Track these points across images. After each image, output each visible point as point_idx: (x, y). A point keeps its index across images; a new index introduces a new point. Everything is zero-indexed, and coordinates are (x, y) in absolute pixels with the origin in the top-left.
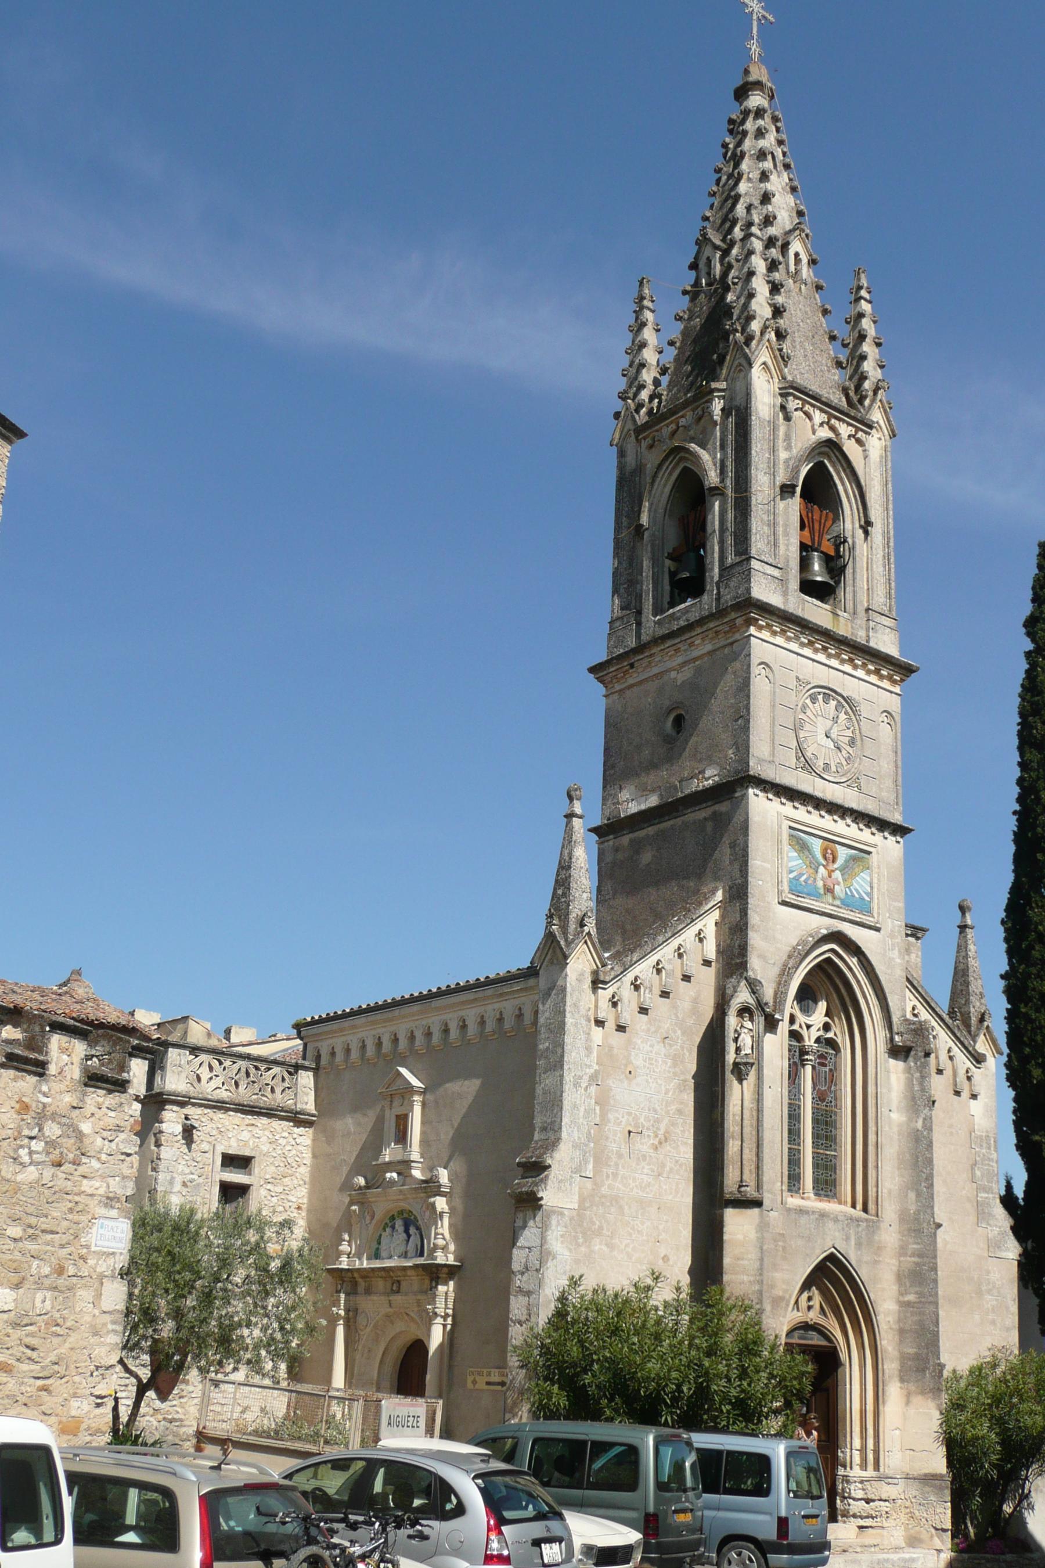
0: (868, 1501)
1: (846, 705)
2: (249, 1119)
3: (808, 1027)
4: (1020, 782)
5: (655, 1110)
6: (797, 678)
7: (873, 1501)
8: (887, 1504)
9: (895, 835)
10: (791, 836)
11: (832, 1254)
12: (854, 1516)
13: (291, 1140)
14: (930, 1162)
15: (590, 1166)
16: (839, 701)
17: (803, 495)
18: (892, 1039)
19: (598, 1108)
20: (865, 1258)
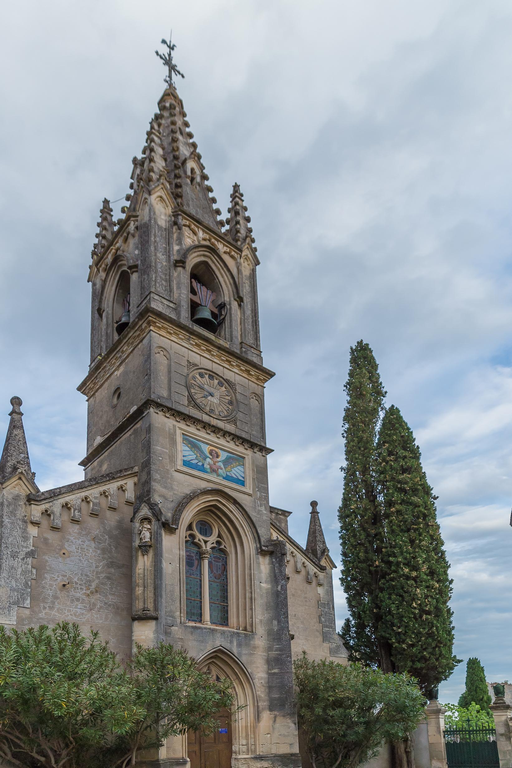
1: (225, 383)
5: (87, 575)
6: (188, 361)
15: (28, 601)
18: (261, 548)
20: (244, 652)
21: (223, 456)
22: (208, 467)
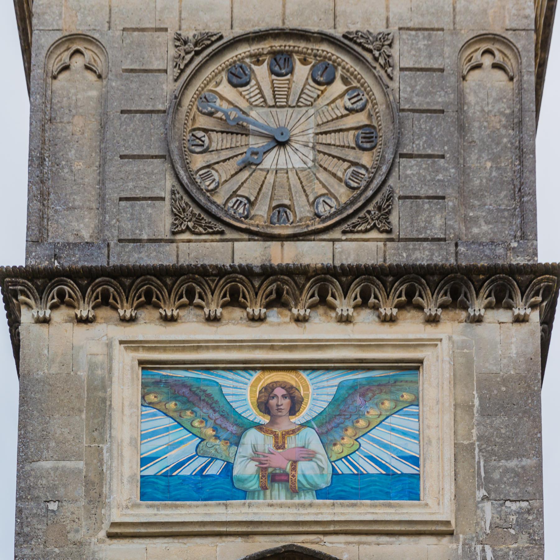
21: (318, 392)
22: (252, 468)
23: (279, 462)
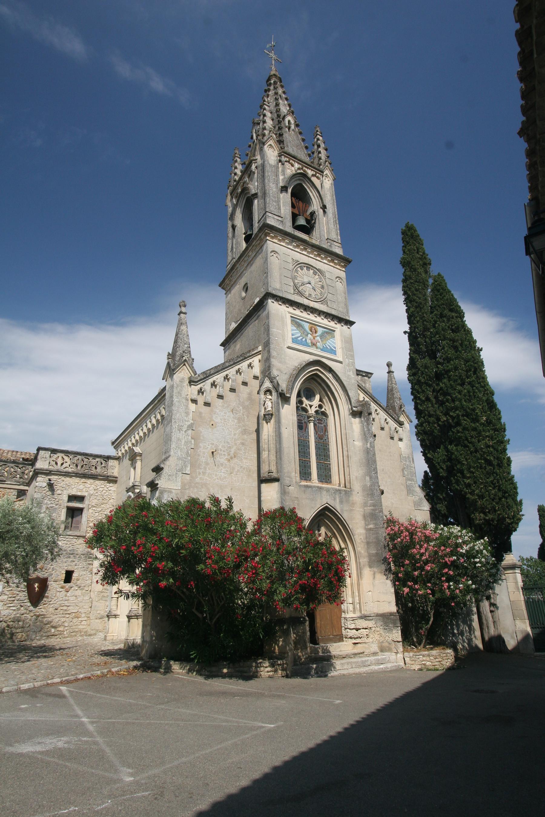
0: (357, 630)
2: (83, 480)
3: (311, 406)
4: (407, 311)
5: (228, 443)
7: (360, 629)
8: (367, 630)
9: (347, 325)
10: (292, 321)
11: (326, 507)
12: (351, 638)
13: (105, 488)
14: (375, 461)
15: (189, 468)
16: (314, 271)
17: (293, 195)
18: (352, 409)
19: (193, 441)
23: (314, 341)
